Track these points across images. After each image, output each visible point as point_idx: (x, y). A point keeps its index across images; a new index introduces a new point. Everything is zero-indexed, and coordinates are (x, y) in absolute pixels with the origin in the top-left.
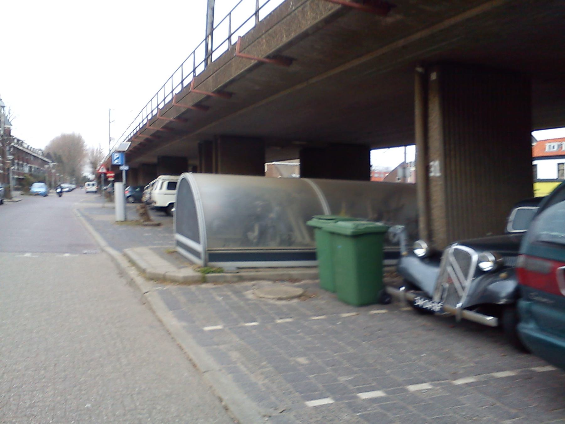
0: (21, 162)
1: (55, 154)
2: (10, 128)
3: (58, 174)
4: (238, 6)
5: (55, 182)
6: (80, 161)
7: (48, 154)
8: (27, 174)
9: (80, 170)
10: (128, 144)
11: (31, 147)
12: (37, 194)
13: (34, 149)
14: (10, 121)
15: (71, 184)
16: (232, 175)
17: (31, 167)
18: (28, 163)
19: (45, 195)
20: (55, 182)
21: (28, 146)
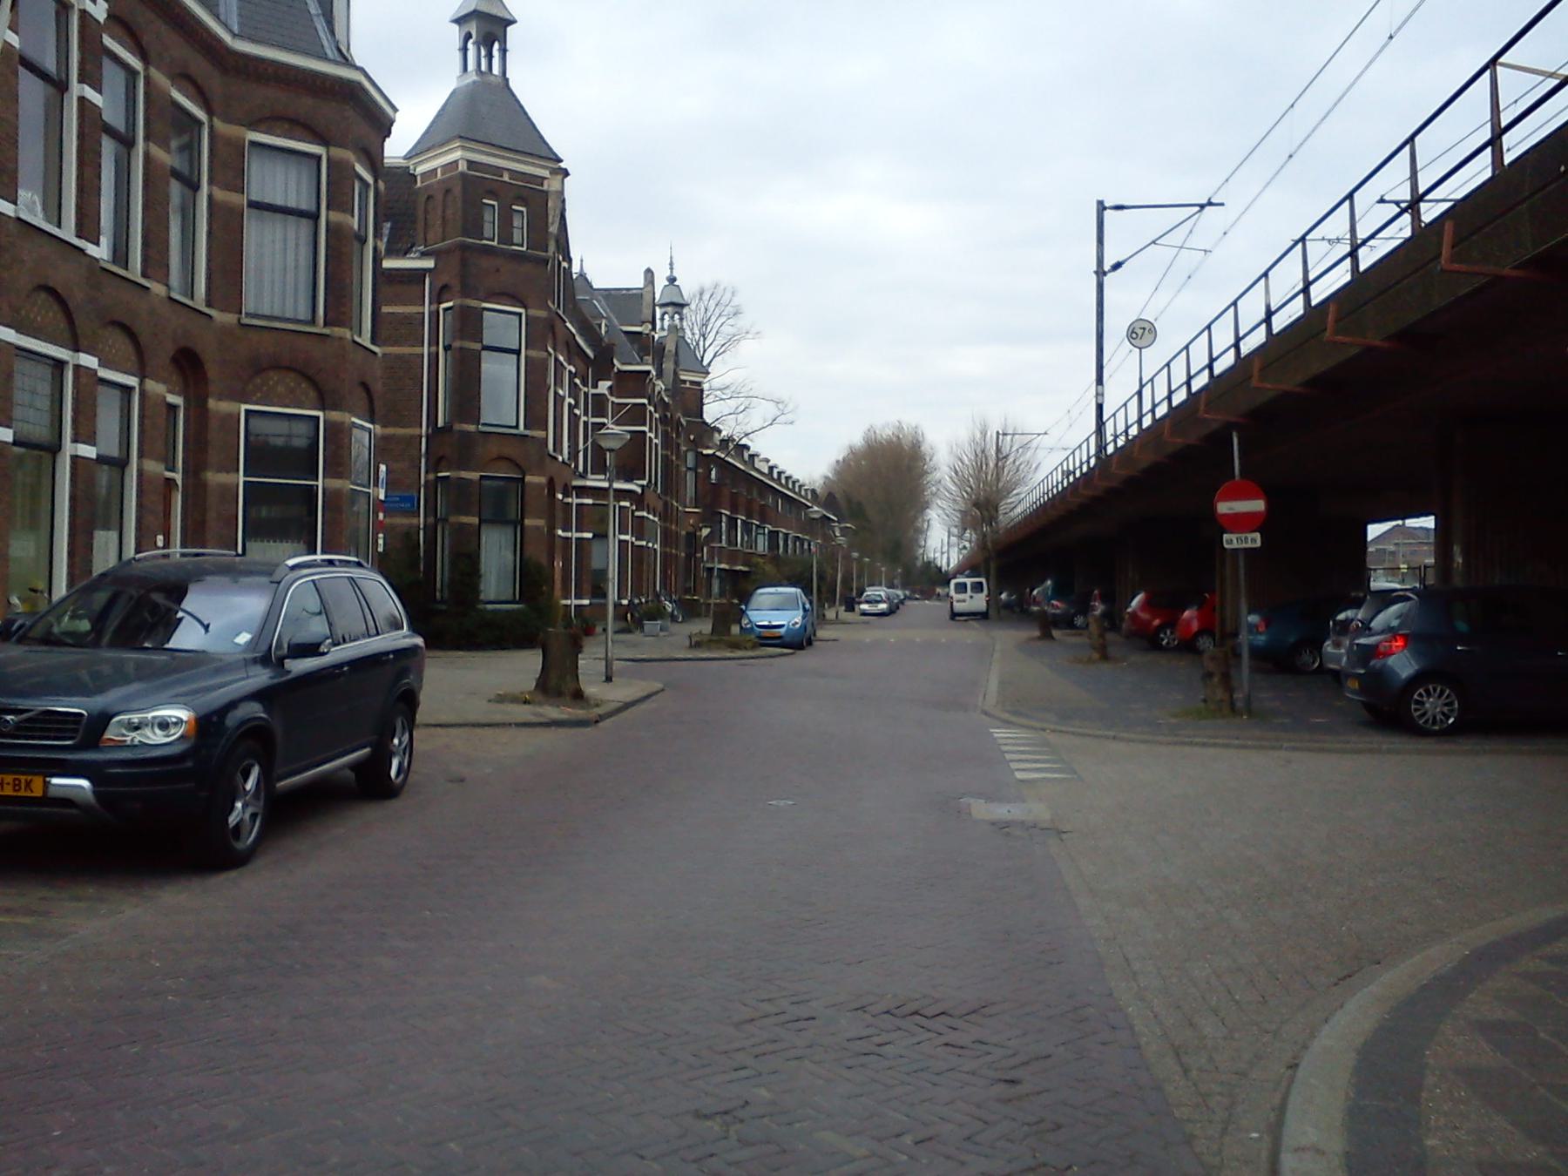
0: (1437, 1073)
1: (849, 501)
2: (699, 384)
3: (855, 555)
4: (1178, 223)
5: (847, 581)
6: (916, 518)
7: (831, 496)
8: (762, 556)
9: (914, 543)
10: (1505, 120)
11: (780, 474)
12: (770, 639)
13: (787, 478)
14: (705, 363)
15: (891, 586)
16: (309, 670)
17: (773, 536)
18: (764, 520)
19: (799, 642)
20: (847, 581)
21: (771, 468)
